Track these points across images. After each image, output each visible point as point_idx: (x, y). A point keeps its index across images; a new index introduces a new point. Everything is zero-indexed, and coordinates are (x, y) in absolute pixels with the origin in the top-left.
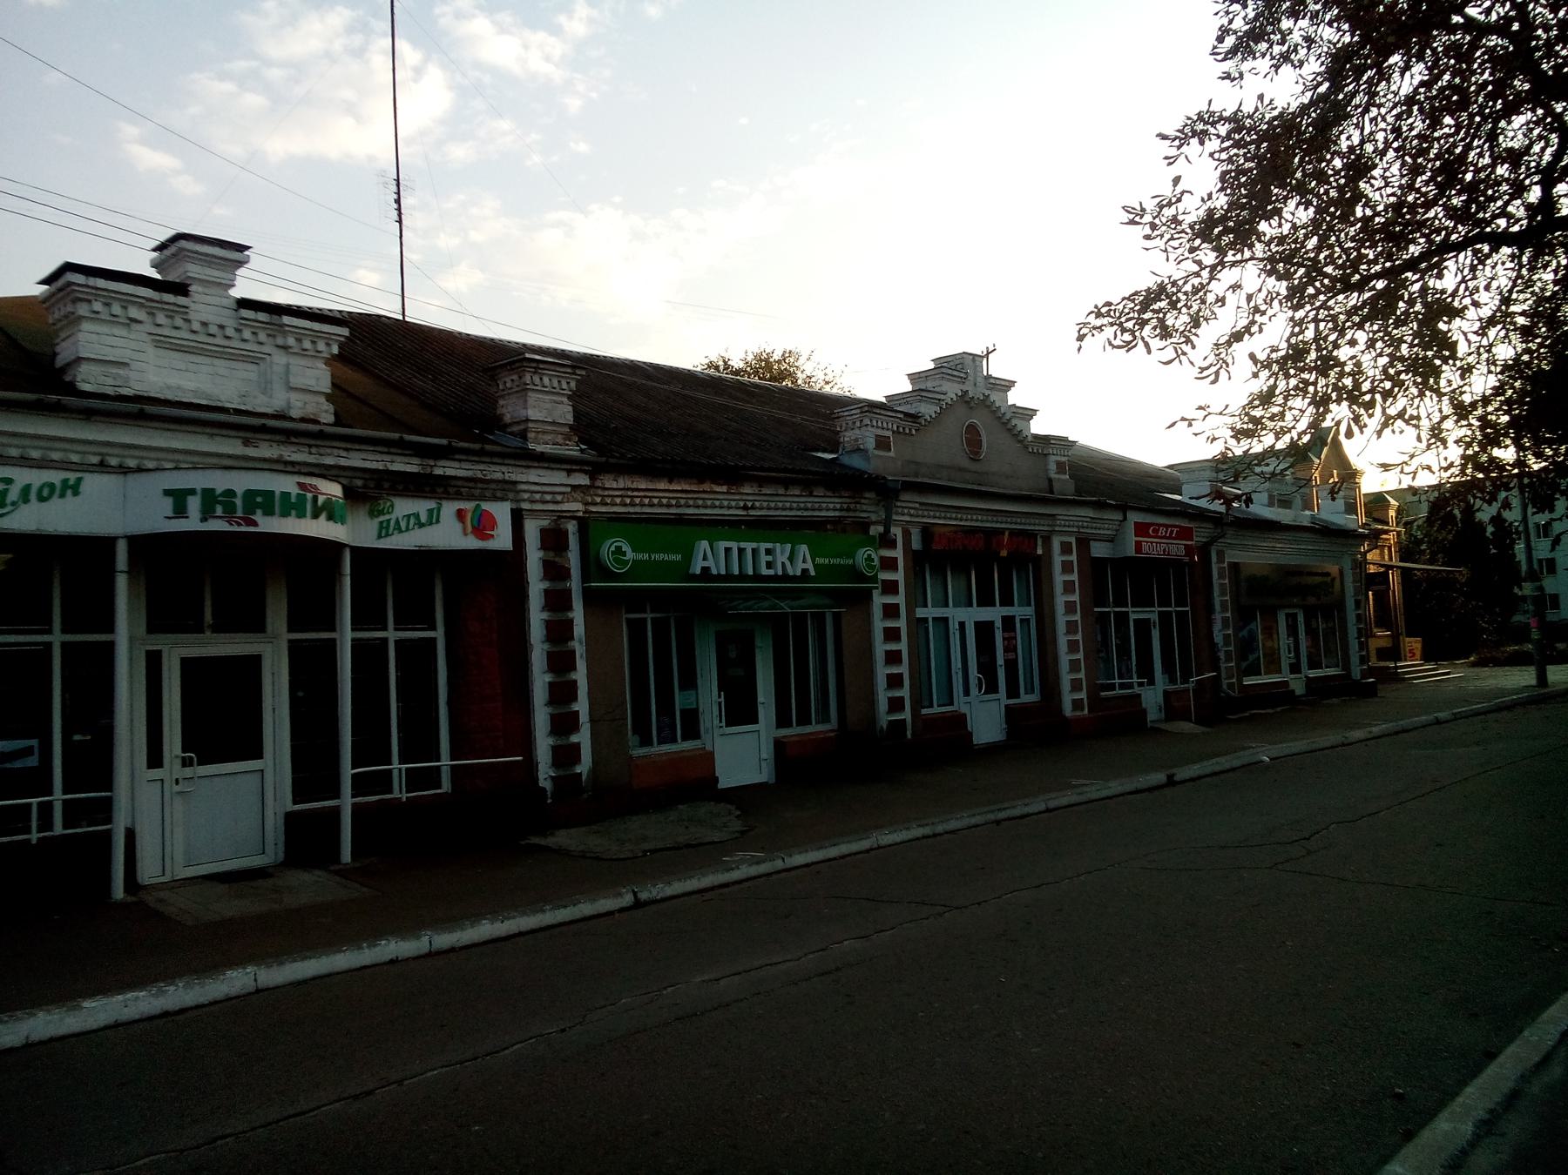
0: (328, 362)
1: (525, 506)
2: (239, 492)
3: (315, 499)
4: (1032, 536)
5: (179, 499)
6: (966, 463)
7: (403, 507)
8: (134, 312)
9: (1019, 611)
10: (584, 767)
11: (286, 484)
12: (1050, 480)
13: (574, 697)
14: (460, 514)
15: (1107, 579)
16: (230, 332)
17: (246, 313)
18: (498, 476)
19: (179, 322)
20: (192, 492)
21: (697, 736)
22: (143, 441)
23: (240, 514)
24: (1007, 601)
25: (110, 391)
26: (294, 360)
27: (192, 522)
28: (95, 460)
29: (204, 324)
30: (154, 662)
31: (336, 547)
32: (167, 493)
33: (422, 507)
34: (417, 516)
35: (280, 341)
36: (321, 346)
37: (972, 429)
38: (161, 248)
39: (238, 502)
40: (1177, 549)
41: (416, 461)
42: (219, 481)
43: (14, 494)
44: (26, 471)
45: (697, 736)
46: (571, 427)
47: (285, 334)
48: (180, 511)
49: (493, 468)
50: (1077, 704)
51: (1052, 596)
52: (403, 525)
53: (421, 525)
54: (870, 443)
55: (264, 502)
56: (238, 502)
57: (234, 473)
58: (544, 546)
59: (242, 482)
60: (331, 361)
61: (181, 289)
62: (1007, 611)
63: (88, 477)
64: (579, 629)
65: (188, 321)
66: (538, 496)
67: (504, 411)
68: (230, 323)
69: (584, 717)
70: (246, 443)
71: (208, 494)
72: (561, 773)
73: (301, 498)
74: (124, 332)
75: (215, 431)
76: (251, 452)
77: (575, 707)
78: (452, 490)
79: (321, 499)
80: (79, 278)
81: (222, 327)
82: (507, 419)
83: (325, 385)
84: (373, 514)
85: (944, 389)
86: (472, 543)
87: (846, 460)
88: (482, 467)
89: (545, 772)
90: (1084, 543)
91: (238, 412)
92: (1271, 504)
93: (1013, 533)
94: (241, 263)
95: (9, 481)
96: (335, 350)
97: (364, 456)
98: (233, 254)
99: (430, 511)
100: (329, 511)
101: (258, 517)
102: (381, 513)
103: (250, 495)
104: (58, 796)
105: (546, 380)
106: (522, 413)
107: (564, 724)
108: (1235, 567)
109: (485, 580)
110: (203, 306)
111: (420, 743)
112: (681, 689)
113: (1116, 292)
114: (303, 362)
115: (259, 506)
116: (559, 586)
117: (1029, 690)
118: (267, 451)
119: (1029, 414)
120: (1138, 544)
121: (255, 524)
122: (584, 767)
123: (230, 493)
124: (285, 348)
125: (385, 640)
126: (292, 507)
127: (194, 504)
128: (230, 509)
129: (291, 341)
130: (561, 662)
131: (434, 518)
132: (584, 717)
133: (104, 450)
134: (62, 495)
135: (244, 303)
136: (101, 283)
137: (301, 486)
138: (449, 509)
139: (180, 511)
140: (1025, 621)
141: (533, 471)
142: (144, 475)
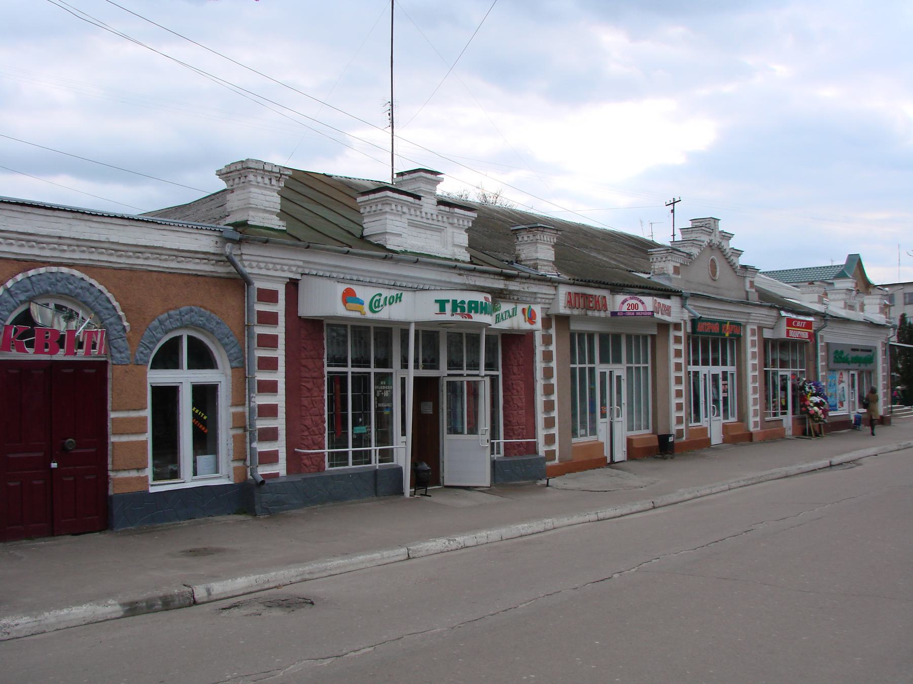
0: (466, 231)
4: (739, 325)
5: (442, 303)
6: (709, 281)
9: (730, 369)
12: (747, 292)
15: (775, 350)
17: (442, 207)
19: (418, 213)
20: (448, 301)
22: (412, 274)
24: (724, 363)
26: (455, 230)
27: (447, 317)
32: (436, 301)
35: (451, 221)
36: (466, 223)
37: (712, 260)
39: (466, 306)
40: (805, 335)
41: (502, 282)
42: (460, 296)
43: (382, 303)
46: (553, 262)
47: (453, 217)
48: (442, 310)
50: (756, 423)
51: (746, 361)
53: (510, 317)
54: (671, 271)
56: (466, 306)
60: (468, 230)
62: (725, 368)
63: (404, 294)
71: (454, 302)
74: (398, 218)
82: (523, 257)
83: (466, 243)
85: (702, 239)
90: (760, 329)
92: (845, 308)
93: (732, 323)
94: (438, 182)
95: (380, 295)
101: (472, 314)
103: (470, 302)
106: (535, 256)
108: (828, 345)
110: (428, 205)
114: (458, 231)
115: (473, 308)
117: (733, 415)
119: (738, 253)
120: (788, 331)
121: (470, 317)
123: (463, 302)
124: (452, 224)
127: (448, 307)
128: (463, 310)
134: (390, 304)
136: (396, 195)
138: (520, 307)
139: (442, 310)
140: (732, 374)
142: (424, 292)
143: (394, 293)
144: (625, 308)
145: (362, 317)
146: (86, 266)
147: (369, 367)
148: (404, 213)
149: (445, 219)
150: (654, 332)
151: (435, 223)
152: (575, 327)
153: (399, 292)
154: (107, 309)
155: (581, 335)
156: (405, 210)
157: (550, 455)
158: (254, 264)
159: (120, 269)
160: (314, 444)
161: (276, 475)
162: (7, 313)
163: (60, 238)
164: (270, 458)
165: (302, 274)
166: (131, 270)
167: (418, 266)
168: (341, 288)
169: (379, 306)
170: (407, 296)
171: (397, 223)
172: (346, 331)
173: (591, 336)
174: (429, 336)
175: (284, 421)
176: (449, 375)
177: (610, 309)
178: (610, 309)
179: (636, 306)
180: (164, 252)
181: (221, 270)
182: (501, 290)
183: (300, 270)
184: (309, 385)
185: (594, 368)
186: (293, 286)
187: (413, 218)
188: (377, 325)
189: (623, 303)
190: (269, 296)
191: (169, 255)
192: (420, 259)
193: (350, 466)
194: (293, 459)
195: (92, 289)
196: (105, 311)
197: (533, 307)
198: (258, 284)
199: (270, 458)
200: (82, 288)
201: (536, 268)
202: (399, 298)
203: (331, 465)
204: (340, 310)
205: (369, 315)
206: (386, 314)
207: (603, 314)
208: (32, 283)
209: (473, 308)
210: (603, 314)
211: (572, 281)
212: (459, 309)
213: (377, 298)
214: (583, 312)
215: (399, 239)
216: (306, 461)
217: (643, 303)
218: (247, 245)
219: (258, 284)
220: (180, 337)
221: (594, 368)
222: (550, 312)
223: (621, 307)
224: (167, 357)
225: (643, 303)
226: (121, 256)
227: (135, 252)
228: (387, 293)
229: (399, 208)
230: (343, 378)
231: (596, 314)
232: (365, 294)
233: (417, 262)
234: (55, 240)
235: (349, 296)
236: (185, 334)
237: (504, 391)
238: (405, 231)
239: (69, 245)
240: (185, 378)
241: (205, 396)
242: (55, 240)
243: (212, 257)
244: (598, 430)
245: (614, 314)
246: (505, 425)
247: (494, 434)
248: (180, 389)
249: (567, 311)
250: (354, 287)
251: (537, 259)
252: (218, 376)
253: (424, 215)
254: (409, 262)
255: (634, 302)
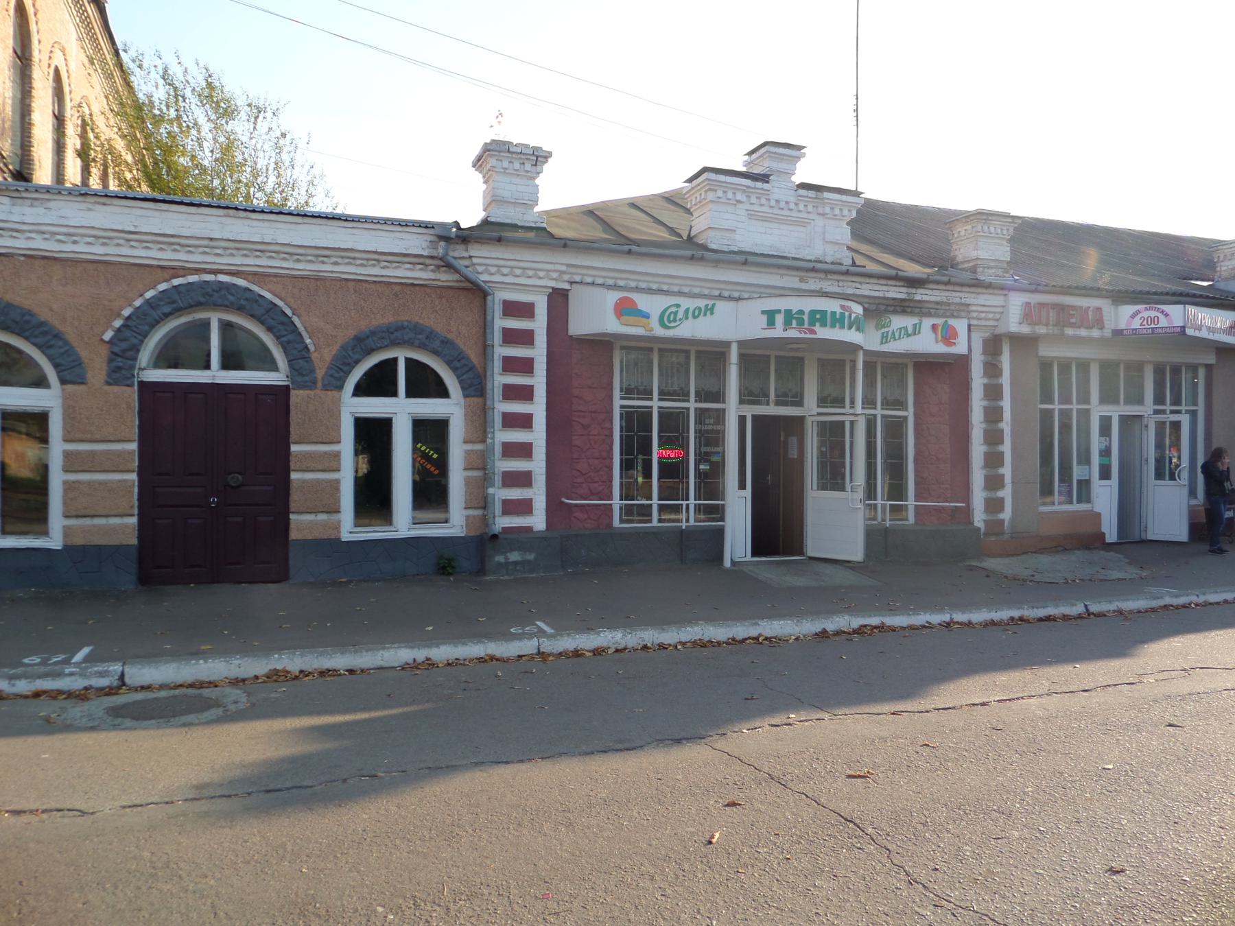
1: (974, 322)
2: (807, 311)
3: (850, 316)
5: (771, 315)
7: (898, 322)
8: (739, 196)
10: (1006, 515)
11: (832, 306)
13: (1001, 464)
14: (934, 327)
16: (792, 206)
18: (958, 300)
19: (763, 201)
20: (779, 312)
21: (1089, 501)
23: (806, 326)
25: (725, 249)
27: (778, 332)
28: (717, 293)
29: (777, 201)
30: (742, 419)
31: (854, 348)
32: (763, 312)
33: (907, 322)
34: (906, 329)
35: (820, 210)
36: (846, 212)
38: (751, 153)
39: (806, 318)
41: (904, 290)
42: (794, 304)
43: (680, 315)
44: (687, 299)
45: (1089, 501)
46: (1008, 263)
48: (771, 323)
49: (954, 294)
52: (897, 335)
53: (909, 335)
55: (819, 317)
56: (806, 318)
57: (783, 299)
58: (985, 352)
59: (809, 305)
61: (764, 178)
64: (1007, 415)
65: (768, 200)
66: (983, 315)
67: (957, 253)
68: (792, 199)
69: (1008, 479)
70: (802, 280)
71: (788, 313)
72: (990, 518)
73: (842, 315)
74: (730, 209)
75: (785, 272)
76: (804, 286)
77: (1001, 471)
78: (917, 310)
79: (853, 316)
80: (712, 176)
81: (787, 203)
82: (960, 259)
84: (878, 328)
86: (941, 348)
87: (1222, 285)
88: (947, 294)
89: (979, 518)
91: (794, 259)
94: (798, 158)
95: (678, 306)
96: (854, 214)
97: (870, 287)
98: (792, 151)
99: (915, 325)
100: (856, 325)
101: (817, 328)
102: (884, 327)
103: (813, 313)
104: (692, 501)
105: (992, 229)
106: (974, 254)
107: (994, 482)
109: (941, 372)
110: (776, 188)
111: (896, 491)
112: (1079, 463)
113: (1227, 461)
115: (818, 320)
116: (994, 381)
118: (813, 284)
121: (814, 332)
122: (1006, 515)
123: (801, 312)
124: (823, 215)
125: (883, 416)
126: (837, 321)
127: (779, 319)
128: (801, 322)
129: (828, 210)
130: (993, 438)
131: (916, 330)
132: (1008, 479)
133: (722, 286)
135: (803, 186)
136: (722, 178)
137: (843, 307)
138: (927, 323)
139: (771, 323)
141: (981, 297)
143: (701, 303)
144: (1136, 324)
145: (648, 334)
146: (255, 274)
147: (688, 401)
148: (739, 202)
149: (810, 208)
150: (1211, 359)
151: (794, 214)
152: (1046, 351)
153: (710, 303)
154: (283, 324)
155: (1065, 366)
156: (739, 196)
157: (995, 527)
158: (493, 270)
159: (303, 277)
160: (592, 494)
161: (528, 530)
162: (147, 328)
163: (211, 239)
164: (524, 507)
165: (571, 283)
166: (318, 279)
167: (746, 268)
168: (613, 297)
169: (675, 320)
170: (721, 306)
171: (726, 216)
172: (688, 358)
173: (1084, 366)
174: (755, 358)
175: (544, 464)
176: (819, 414)
177: (1110, 325)
178: (1110, 325)
179: (1154, 320)
180: (357, 255)
181: (445, 277)
182: (902, 300)
183: (566, 277)
184: (585, 421)
185: (1088, 411)
186: (559, 300)
187: (751, 207)
188: (700, 348)
189: (1133, 316)
190: (526, 310)
191: (368, 260)
192: (750, 258)
193: (655, 523)
194: (554, 507)
195: (260, 300)
196: (281, 327)
197: (952, 322)
198: (501, 295)
199: (524, 507)
200: (246, 299)
201: (975, 272)
202: (710, 310)
203: (622, 521)
204: (612, 325)
205: (659, 332)
206: (686, 330)
207: (1096, 333)
208: (179, 293)
209: (818, 320)
210: (1096, 333)
211: (1033, 287)
212: (794, 322)
213: (673, 309)
214: (1056, 330)
215: (732, 235)
216: (578, 514)
217: (1167, 315)
218: (477, 246)
219: (501, 295)
220: (395, 360)
221: (1088, 411)
222: (998, 332)
223: (1129, 323)
224: (378, 383)
225: (1167, 315)
226: (298, 261)
227: (317, 256)
228: (687, 303)
229: (730, 195)
230: (646, 416)
231: (1083, 332)
232: (652, 305)
233: (745, 263)
234: (205, 243)
235: (625, 309)
236: (401, 355)
237: (916, 438)
238: (740, 225)
239: (225, 248)
240: (401, 410)
241: (431, 433)
242: (205, 243)
243: (428, 261)
244: (1093, 495)
245: (1118, 333)
246: (917, 484)
247: (870, 492)
248: (394, 420)
249: (1025, 329)
250: (635, 297)
251: (977, 259)
252: (450, 408)
253: (773, 203)
254: (735, 263)
255: (1153, 314)
